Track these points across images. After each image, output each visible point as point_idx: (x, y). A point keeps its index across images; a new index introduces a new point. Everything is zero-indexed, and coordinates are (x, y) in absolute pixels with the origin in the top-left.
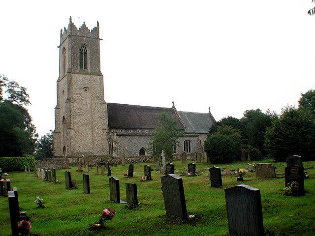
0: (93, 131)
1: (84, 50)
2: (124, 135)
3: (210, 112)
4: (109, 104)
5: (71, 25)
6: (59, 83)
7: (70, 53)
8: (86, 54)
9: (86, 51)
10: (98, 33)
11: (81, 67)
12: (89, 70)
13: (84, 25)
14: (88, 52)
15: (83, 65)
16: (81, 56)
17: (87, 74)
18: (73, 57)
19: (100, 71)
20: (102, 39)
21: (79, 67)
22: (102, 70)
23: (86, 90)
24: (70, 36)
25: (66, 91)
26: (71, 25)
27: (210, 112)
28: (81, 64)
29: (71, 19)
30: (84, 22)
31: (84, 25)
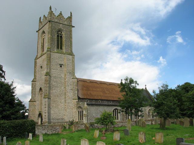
0: (65, 101)
1: (60, 34)
2: (92, 105)
3: (146, 88)
4: (80, 81)
5: (51, 13)
6: (37, 60)
7: (50, 35)
8: (61, 37)
9: (62, 35)
10: (71, 21)
11: (58, 48)
12: (64, 50)
13: (61, 14)
14: (64, 36)
15: (60, 46)
16: (58, 38)
17: (62, 53)
18: (52, 39)
19: (72, 51)
20: (74, 27)
21: (56, 47)
22: (73, 51)
23: (61, 66)
24: (50, 21)
25: (45, 66)
26: (51, 13)
27: (146, 88)
28: (58, 43)
29: (50, 8)
30: (61, 12)
31: (61, 14)
